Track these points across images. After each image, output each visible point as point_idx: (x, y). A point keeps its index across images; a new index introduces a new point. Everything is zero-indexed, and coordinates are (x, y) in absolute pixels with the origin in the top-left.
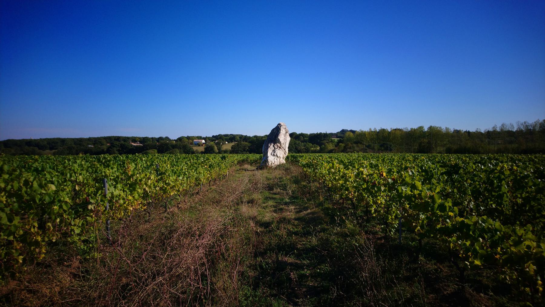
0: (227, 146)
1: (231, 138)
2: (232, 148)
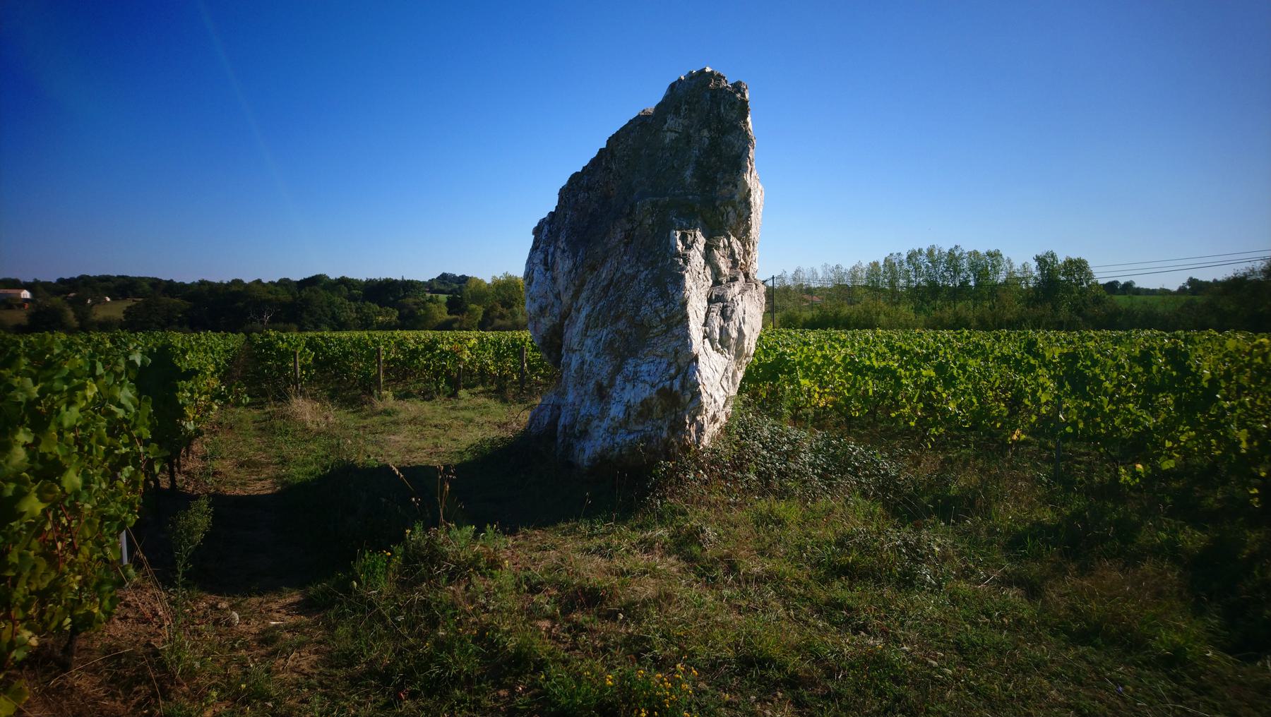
0: (112, 309)
1: (123, 287)
2: (127, 313)
